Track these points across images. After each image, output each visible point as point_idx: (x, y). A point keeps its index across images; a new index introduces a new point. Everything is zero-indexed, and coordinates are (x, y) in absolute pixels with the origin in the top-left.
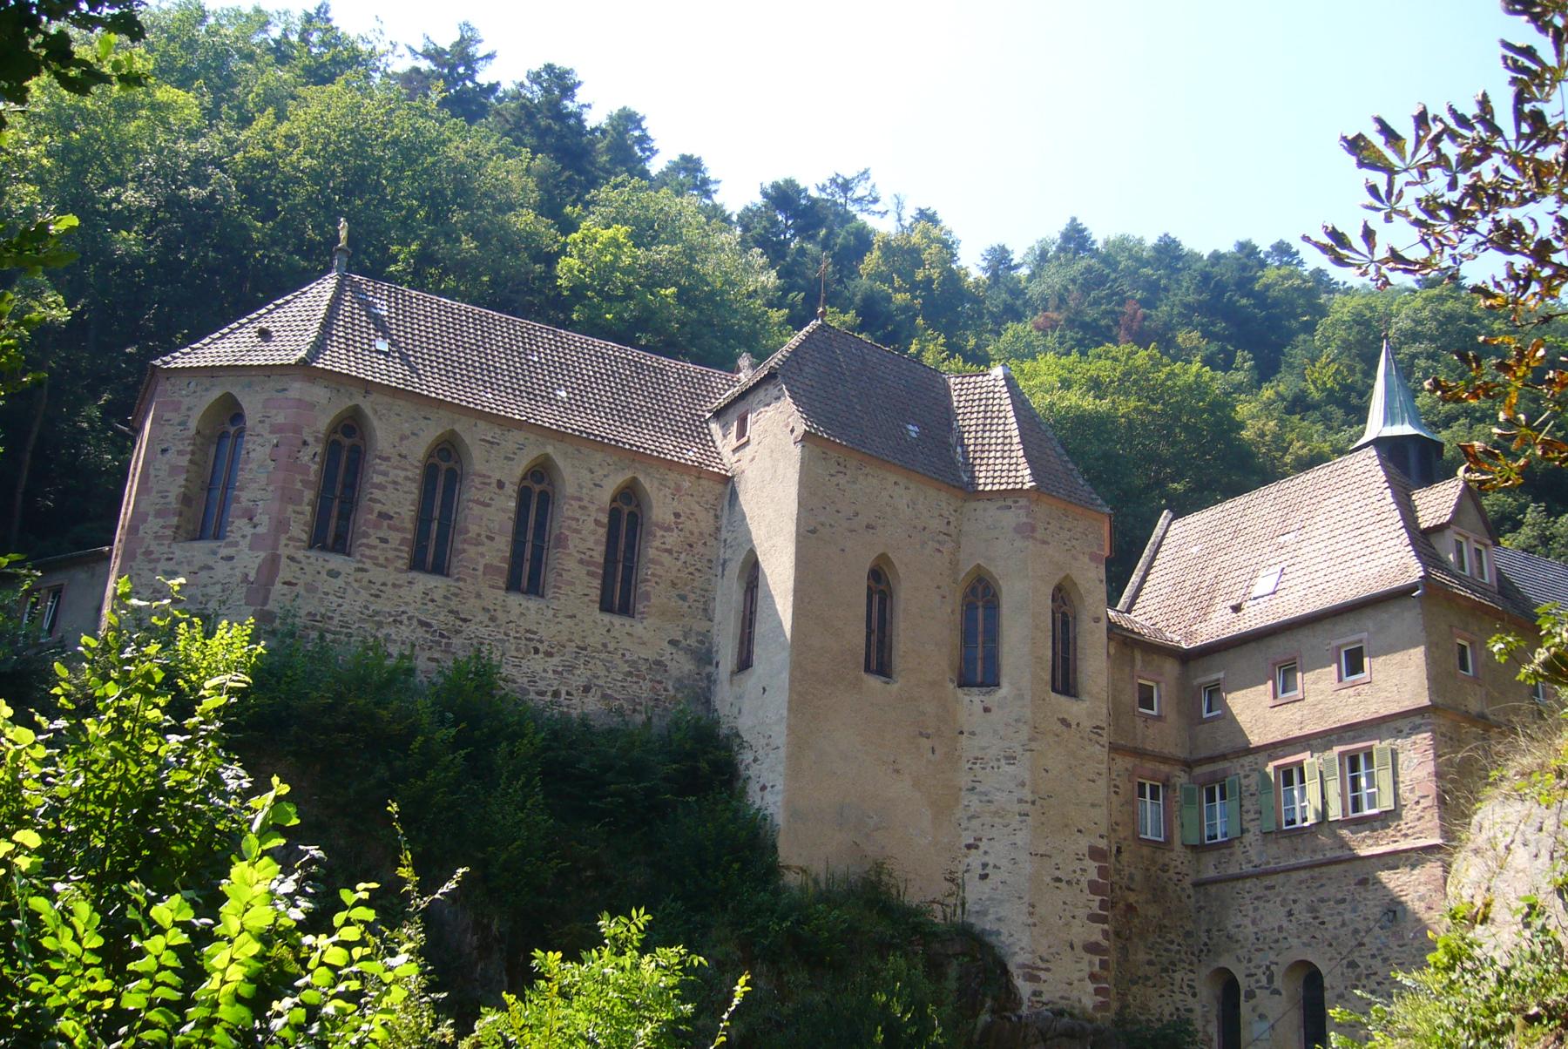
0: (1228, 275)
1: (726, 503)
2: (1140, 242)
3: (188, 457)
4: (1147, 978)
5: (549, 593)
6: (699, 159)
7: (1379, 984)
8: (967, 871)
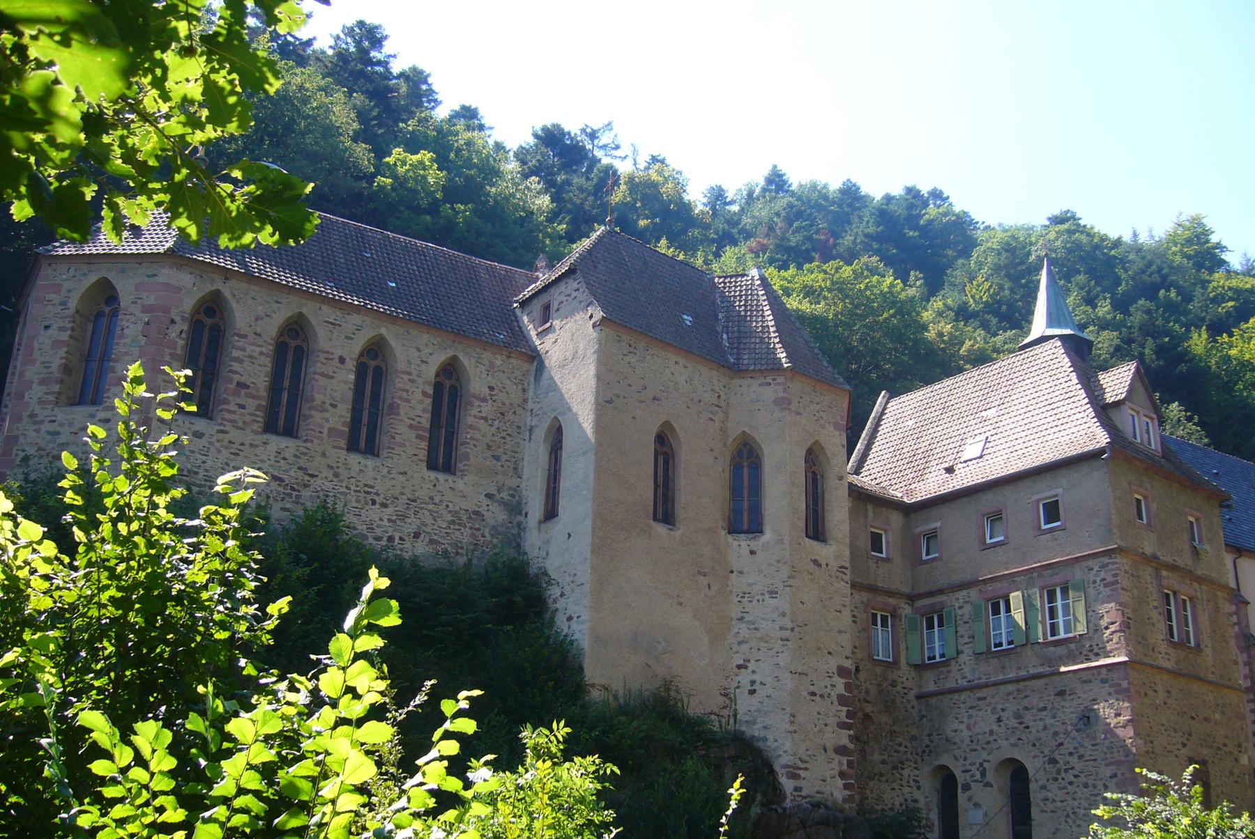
0: (901, 211)
1: (532, 379)
2: (825, 186)
3: (69, 333)
4: (881, 775)
5: (384, 453)
6: (476, 109)
7: (1076, 776)
8: (738, 687)
